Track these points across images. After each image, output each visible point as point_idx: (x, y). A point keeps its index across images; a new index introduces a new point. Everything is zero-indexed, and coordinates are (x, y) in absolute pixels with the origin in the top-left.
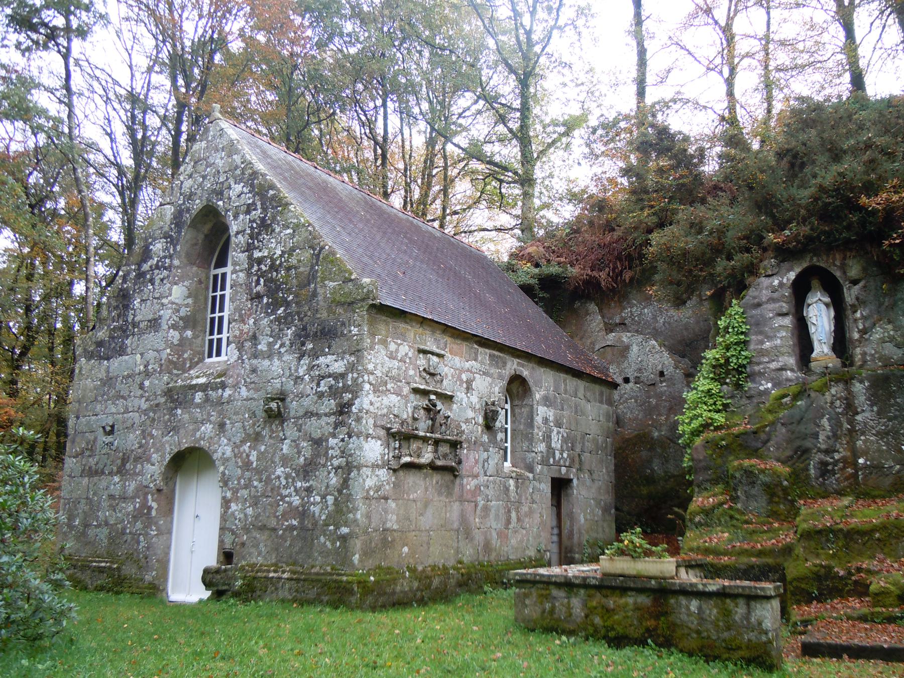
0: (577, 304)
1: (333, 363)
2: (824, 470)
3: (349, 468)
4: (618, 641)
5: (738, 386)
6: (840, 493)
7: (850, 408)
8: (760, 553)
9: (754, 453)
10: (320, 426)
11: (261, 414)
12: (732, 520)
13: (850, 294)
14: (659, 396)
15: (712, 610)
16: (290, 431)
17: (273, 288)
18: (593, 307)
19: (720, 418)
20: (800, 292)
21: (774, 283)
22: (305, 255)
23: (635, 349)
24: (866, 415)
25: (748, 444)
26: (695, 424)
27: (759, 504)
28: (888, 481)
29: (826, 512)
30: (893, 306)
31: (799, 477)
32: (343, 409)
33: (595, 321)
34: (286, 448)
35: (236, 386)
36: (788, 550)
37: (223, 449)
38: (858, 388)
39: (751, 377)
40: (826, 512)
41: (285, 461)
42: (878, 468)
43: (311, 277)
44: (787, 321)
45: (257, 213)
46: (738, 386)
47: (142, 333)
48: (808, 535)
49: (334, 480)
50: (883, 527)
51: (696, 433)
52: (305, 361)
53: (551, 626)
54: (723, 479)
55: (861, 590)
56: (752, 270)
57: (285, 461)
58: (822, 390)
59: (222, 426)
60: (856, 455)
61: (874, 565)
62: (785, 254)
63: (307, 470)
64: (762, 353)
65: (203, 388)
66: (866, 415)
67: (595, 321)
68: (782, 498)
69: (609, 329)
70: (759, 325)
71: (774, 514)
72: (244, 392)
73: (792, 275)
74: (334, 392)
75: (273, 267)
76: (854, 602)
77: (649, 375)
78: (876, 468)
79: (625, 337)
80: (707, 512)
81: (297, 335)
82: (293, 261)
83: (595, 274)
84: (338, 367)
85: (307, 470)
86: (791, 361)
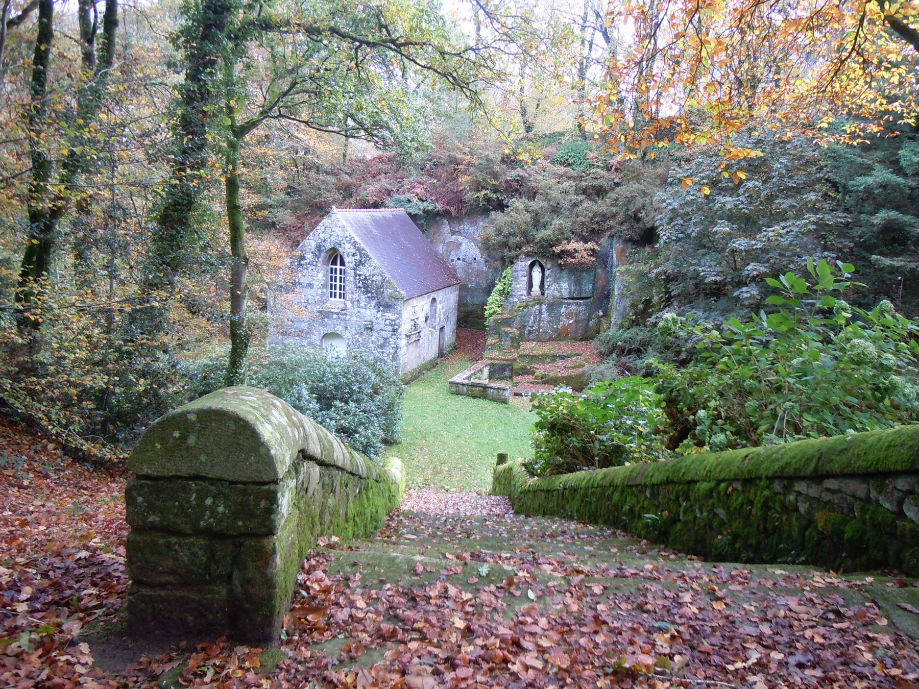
0: (438, 218)
1: (390, 315)
2: (530, 332)
3: (397, 348)
4: (474, 397)
5: (506, 298)
6: (533, 340)
7: (540, 313)
8: (507, 360)
9: (509, 325)
10: (387, 334)
11: (362, 326)
12: (500, 348)
13: (547, 273)
14: (473, 269)
15: (496, 392)
16: (375, 334)
17: (366, 287)
18: (445, 221)
19: (499, 310)
20: (532, 266)
21: (523, 264)
22: (380, 278)
23: (464, 245)
24: (545, 315)
25: (507, 322)
26: (491, 311)
27: (509, 343)
28: (548, 337)
29: (530, 347)
30: (559, 278)
31: (521, 334)
32: (394, 331)
33: (446, 228)
34: (373, 338)
35: (351, 315)
36: (515, 360)
37: (347, 335)
38: (544, 307)
39: (512, 296)
40: (530, 347)
41: (373, 342)
42: (545, 332)
43: (382, 287)
44: (526, 279)
45: (358, 257)
46: (506, 298)
47: (303, 287)
48: (521, 356)
49: (392, 351)
50: (542, 355)
51: (491, 315)
52: (380, 313)
53: (458, 393)
54: (498, 333)
55: (533, 373)
56: (517, 257)
57: (373, 342)
58: (533, 306)
59: (346, 328)
60: (539, 328)
61: (538, 366)
62: (528, 255)
63: (382, 346)
64: (516, 288)
65: (337, 314)
66: (545, 315)
67: (446, 228)
68: (516, 342)
69: (453, 233)
70: (516, 278)
71: (512, 346)
72: (355, 318)
73: (529, 262)
74: (391, 325)
75: (365, 279)
76: (530, 377)
77: (469, 259)
78: (545, 332)
79: (460, 239)
80: (492, 345)
81: (377, 304)
82: (374, 279)
83: (448, 208)
84: (393, 317)
85: (382, 346)
86: (525, 293)
